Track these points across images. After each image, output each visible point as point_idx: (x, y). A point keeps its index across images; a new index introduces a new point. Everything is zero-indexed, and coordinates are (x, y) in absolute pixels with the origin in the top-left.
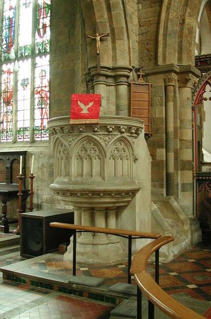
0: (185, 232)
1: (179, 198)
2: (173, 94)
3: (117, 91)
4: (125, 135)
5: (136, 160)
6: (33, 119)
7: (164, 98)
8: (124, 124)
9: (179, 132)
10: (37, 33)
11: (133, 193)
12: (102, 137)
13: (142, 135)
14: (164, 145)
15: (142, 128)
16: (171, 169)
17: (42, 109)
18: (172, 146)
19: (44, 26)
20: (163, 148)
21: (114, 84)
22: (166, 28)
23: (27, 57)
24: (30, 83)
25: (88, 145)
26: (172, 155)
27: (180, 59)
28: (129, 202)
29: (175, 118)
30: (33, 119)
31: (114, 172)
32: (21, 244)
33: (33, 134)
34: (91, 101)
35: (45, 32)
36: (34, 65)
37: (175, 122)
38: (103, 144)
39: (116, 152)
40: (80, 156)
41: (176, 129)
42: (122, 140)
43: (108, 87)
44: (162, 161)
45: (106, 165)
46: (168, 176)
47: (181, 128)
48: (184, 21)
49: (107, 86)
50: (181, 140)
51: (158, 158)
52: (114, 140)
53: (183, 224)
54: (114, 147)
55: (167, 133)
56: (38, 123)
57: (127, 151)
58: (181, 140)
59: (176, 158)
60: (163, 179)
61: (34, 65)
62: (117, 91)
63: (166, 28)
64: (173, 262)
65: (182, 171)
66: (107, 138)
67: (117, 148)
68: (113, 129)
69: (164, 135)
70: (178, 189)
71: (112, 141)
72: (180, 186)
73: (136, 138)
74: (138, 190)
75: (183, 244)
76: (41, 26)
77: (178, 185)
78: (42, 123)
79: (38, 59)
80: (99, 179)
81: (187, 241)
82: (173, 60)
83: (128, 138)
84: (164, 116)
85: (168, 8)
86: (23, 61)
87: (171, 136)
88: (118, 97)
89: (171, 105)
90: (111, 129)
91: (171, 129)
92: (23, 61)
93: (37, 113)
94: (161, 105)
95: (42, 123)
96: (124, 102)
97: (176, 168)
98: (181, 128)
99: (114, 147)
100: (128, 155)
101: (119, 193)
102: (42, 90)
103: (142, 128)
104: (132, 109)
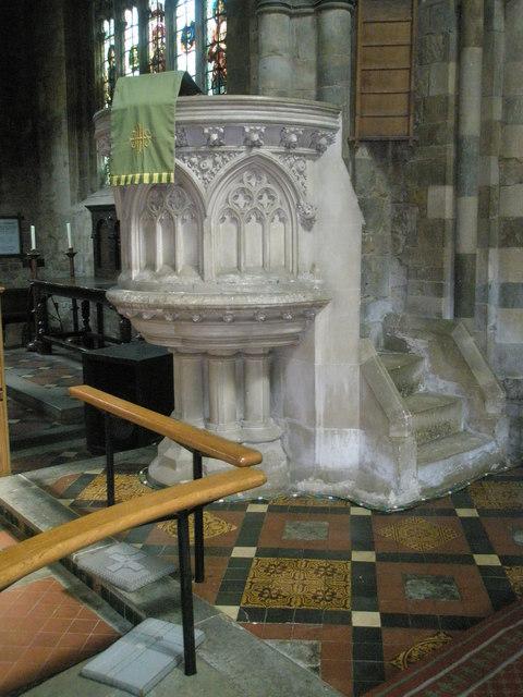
0: (491, 423)
1: (492, 321)
2: (481, 21)
3: (318, 26)
4: (265, 151)
5: (308, 223)
7: (453, 36)
8: (256, 118)
9: (498, 134)
11: (304, 314)
12: (194, 159)
13: (336, 149)
14: (450, 174)
15: (335, 130)
16: (468, 244)
18: (469, 179)
20: (444, 183)
21: (312, 10)
24: (151, 33)
25: (253, 181)
26: (470, 204)
28: (295, 337)
29: (486, 94)
31: (235, 255)
37: (485, 109)
38: (197, 179)
39: (241, 200)
40: (230, 211)
41: (487, 127)
42: (260, 166)
43: (295, 20)
44: (442, 222)
45: (206, 237)
46: (460, 264)
47: (504, 123)
49: (291, 16)
50: (504, 160)
51: (432, 214)
52: (228, 166)
53: (484, 400)
54: (234, 185)
55: (458, 141)
57: (279, 196)
58: (504, 160)
59: (485, 211)
60: (441, 272)
62: (318, 26)
64: (409, 510)
65: (503, 250)
66: (208, 163)
67: (243, 190)
68: (261, 134)
69: (451, 146)
70: (486, 299)
71: (222, 172)
72: (495, 293)
73: (314, 157)
74: (318, 305)
75: (471, 458)
77: (487, 287)
80: (194, 279)
81: (488, 448)
83: (275, 158)
84: (451, 90)
87: (472, 149)
88: (321, 45)
89: (474, 55)
90: (256, 137)
91: (472, 125)
94: (445, 59)
96: (339, 58)
97: (485, 241)
98: (504, 123)
99: (234, 185)
100: (285, 208)
101: (275, 315)
103: (335, 130)
104: (359, 74)
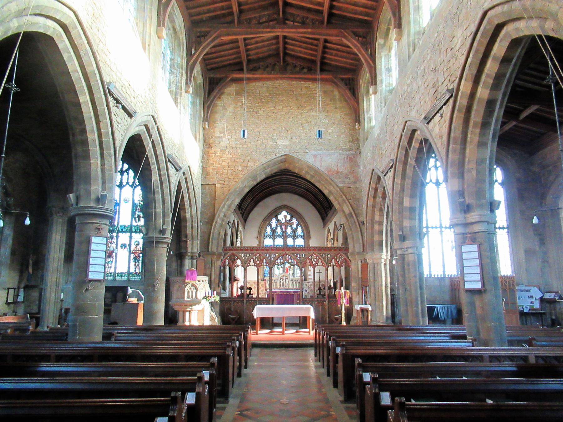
6: (129, 268)
10: (134, 220)
17: (136, 262)
19: (139, 217)
22: (213, 236)
23: (126, 232)
27: (217, 249)
30: (129, 268)
32: (145, 324)
33: (114, 276)
34: (33, 272)
35: (139, 220)
36: (131, 237)
48: (220, 233)
56: (132, 270)
61: (131, 237)
63: (213, 236)
76: (136, 216)
78: (135, 270)
79: (133, 234)
82: (215, 250)
85: (214, 228)
86: (504, 275)
89: (213, 268)
92: (504, 275)
93: (132, 264)
95: (135, 270)
102: (136, 252)
